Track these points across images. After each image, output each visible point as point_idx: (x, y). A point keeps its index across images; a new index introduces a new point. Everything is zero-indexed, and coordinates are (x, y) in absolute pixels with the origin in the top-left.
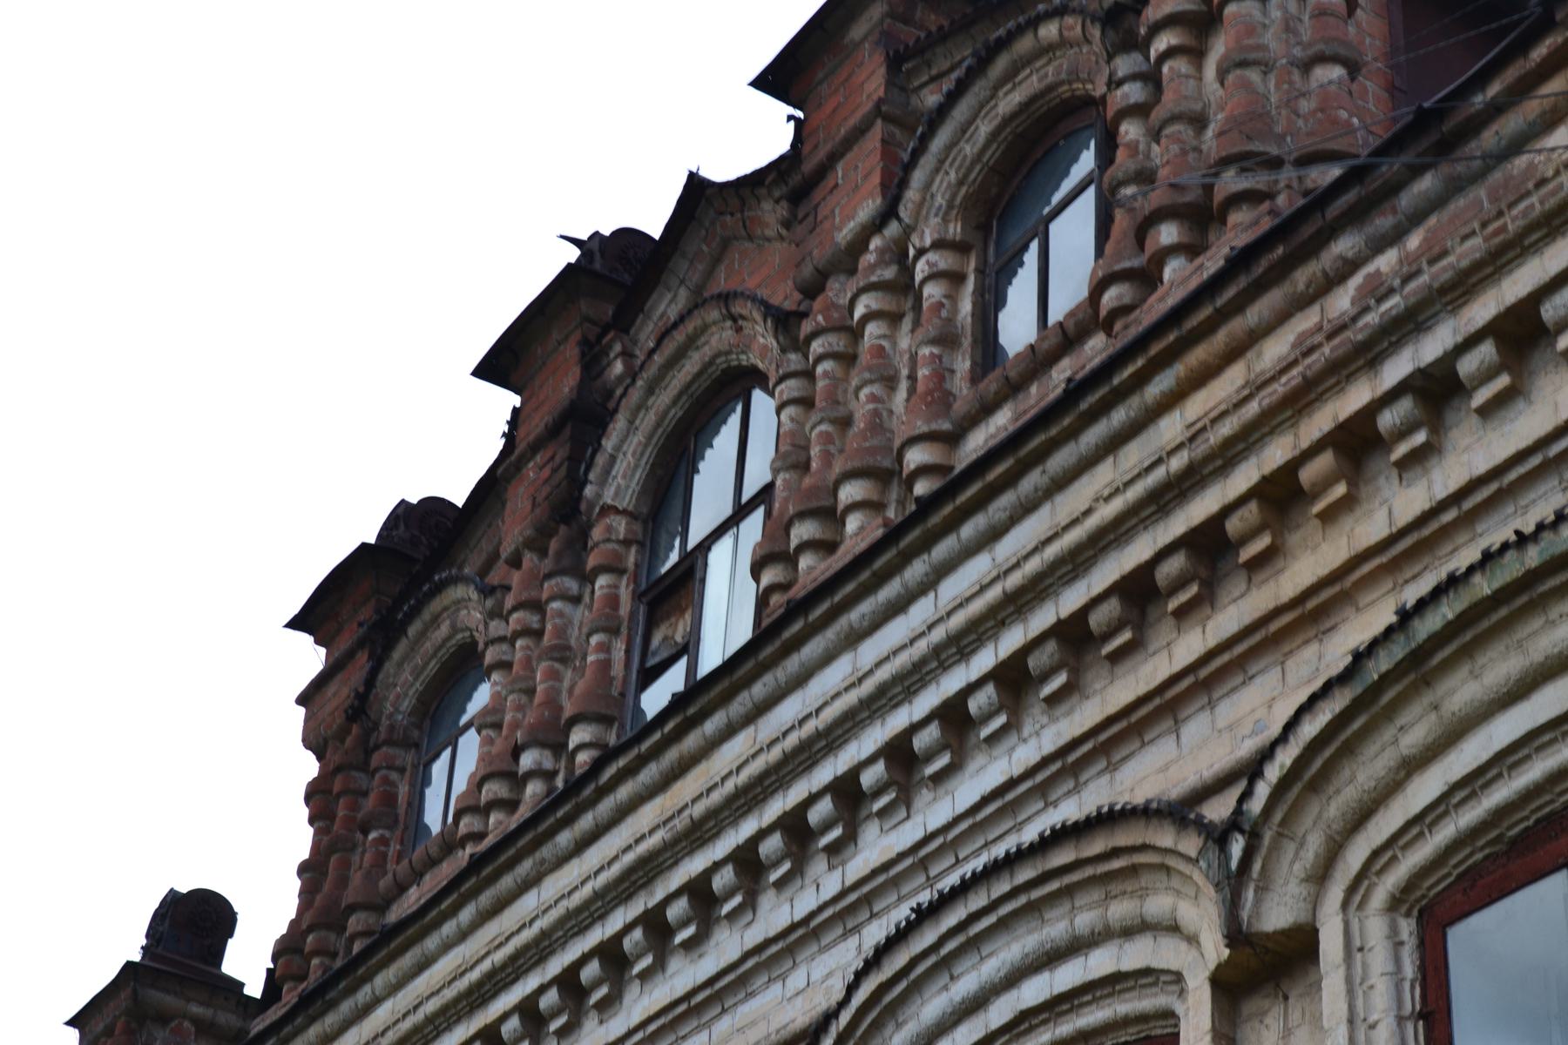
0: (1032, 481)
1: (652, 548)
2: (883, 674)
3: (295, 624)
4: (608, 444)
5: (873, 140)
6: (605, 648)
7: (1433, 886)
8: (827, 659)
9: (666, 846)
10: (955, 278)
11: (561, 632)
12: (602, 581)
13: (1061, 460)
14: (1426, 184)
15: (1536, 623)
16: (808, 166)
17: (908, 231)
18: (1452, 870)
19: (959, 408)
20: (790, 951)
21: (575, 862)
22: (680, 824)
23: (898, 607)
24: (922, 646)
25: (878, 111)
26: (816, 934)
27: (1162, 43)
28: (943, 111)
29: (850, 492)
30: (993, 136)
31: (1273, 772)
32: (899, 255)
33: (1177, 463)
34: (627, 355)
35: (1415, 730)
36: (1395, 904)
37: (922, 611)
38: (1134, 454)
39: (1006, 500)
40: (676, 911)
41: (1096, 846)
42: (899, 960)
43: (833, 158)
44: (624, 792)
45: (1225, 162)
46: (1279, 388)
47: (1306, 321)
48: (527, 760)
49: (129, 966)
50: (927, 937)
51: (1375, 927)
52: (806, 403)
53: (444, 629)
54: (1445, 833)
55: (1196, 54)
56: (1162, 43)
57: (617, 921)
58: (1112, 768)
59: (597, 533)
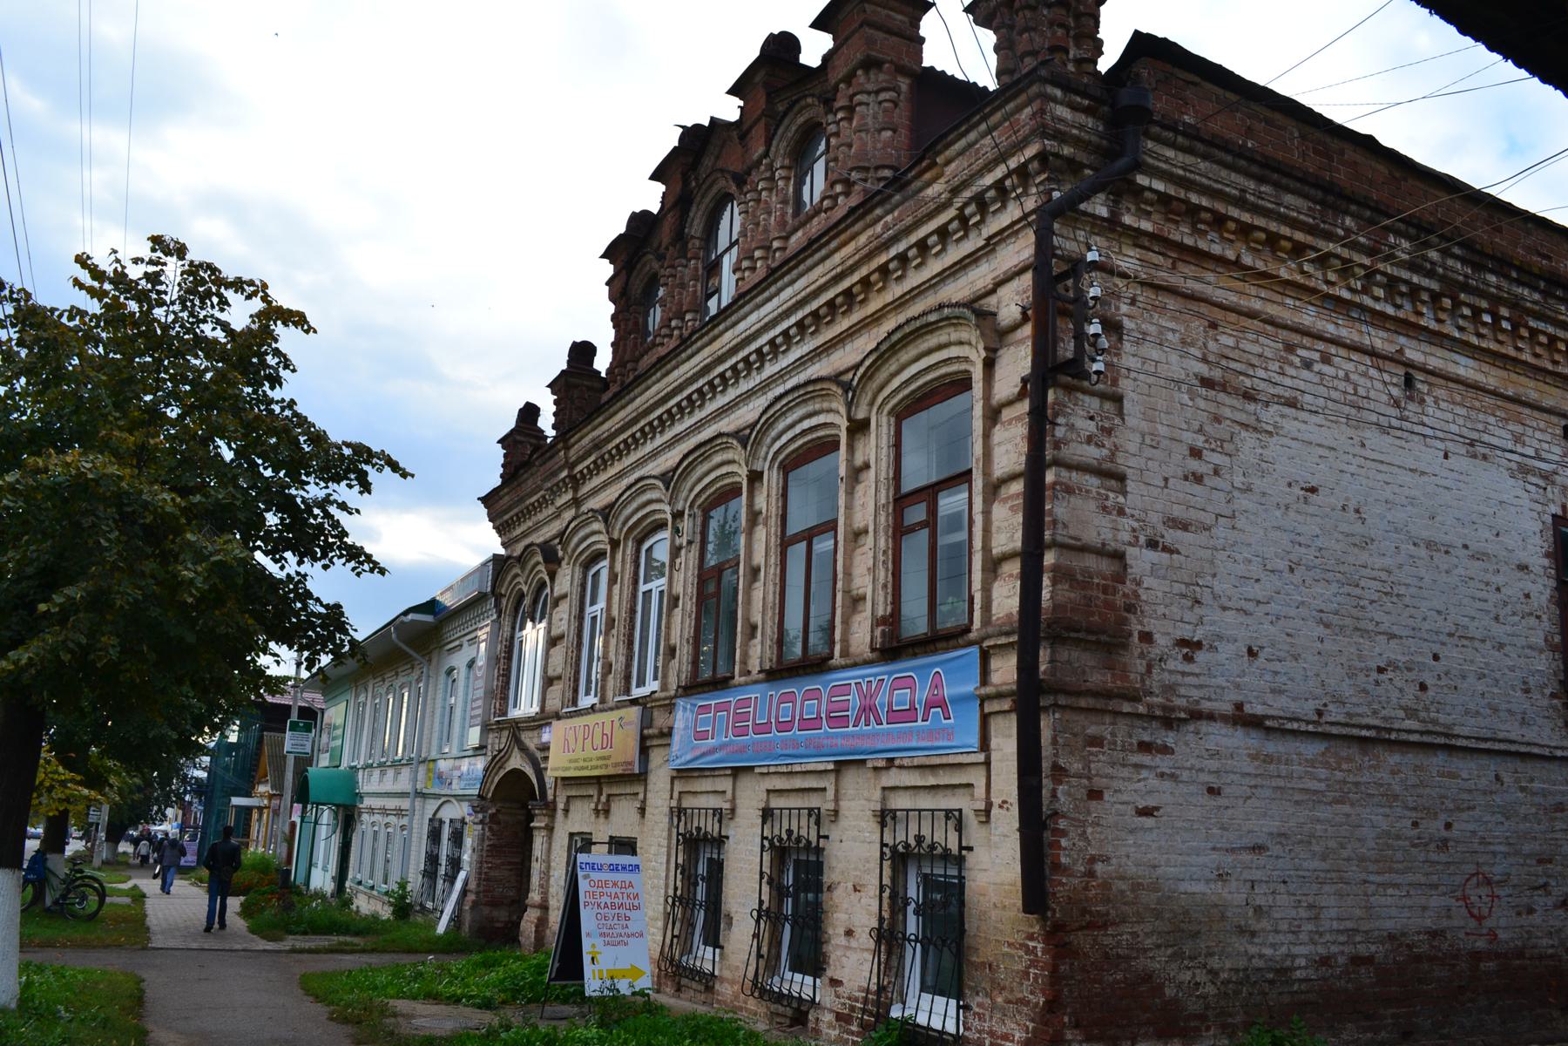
0: (802, 267)
1: (708, 252)
2: (766, 320)
3: (602, 257)
4: (691, 214)
5: (762, 124)
6: (695, 286)
7: (899, 409)
8: (751, 312)
9: (712, 362)
10: (787, 179)
11: (681, 278)
12: (693, 262)
13: (809, 262)
14: (897, 197)
15: (920, 341)
16: (745, 127)
17: (772, 161)
18: (904, 404)
19: (788, 228)
20: (749, 397)
21: (821, 266)
22: (715, 356)
23: (769, 299)
24: (776, 313)
25: (763, 114)
26: (755, 393)
27: (840, 115)
28: (785, 114)
29: (758, 254)
30: (797, 131)
31: (862, 370)
32: (770, 167)
33: (839, 270)
34: (696, 179)
35: (893, 366)
36: (889, 413)
37: (775, 302)
38: (829, 264)
39: (795, 272)
40: (779, 340)
41: (818, 387)
42: (771, 412)
43: (751, 127)
44: (699, 344)
45: (852, 169)
46: (863, 252)
47: (870, 232)
48: (673, 323)
49: (563, 371)
50: (778, 406)
51: (884, 420)
52: (747, 212)
53: (648, 268)
54: (900, 396)
55: (849, 119)
56: (840, 115)
57: (701, 382)
58: (828, 355)
59: (690, 246)
